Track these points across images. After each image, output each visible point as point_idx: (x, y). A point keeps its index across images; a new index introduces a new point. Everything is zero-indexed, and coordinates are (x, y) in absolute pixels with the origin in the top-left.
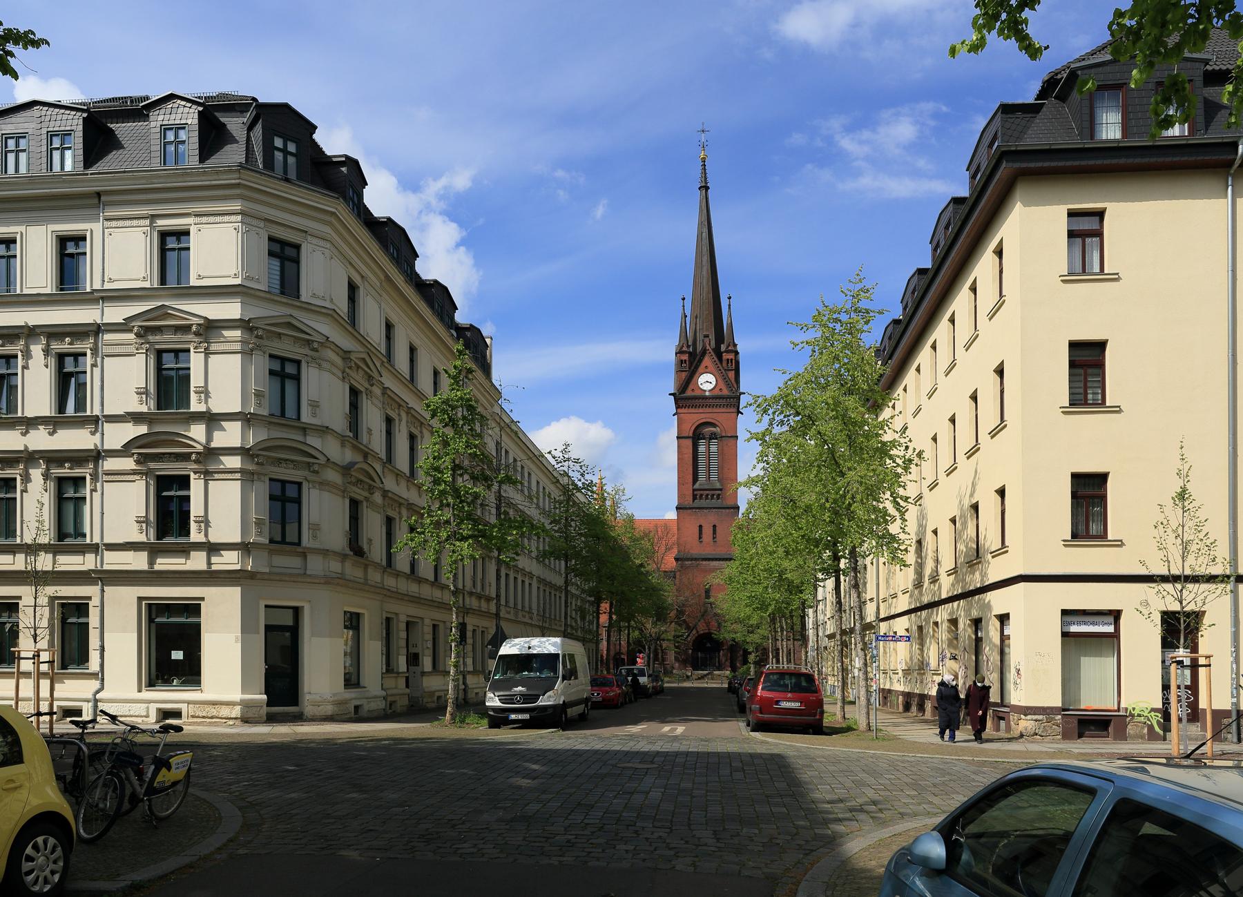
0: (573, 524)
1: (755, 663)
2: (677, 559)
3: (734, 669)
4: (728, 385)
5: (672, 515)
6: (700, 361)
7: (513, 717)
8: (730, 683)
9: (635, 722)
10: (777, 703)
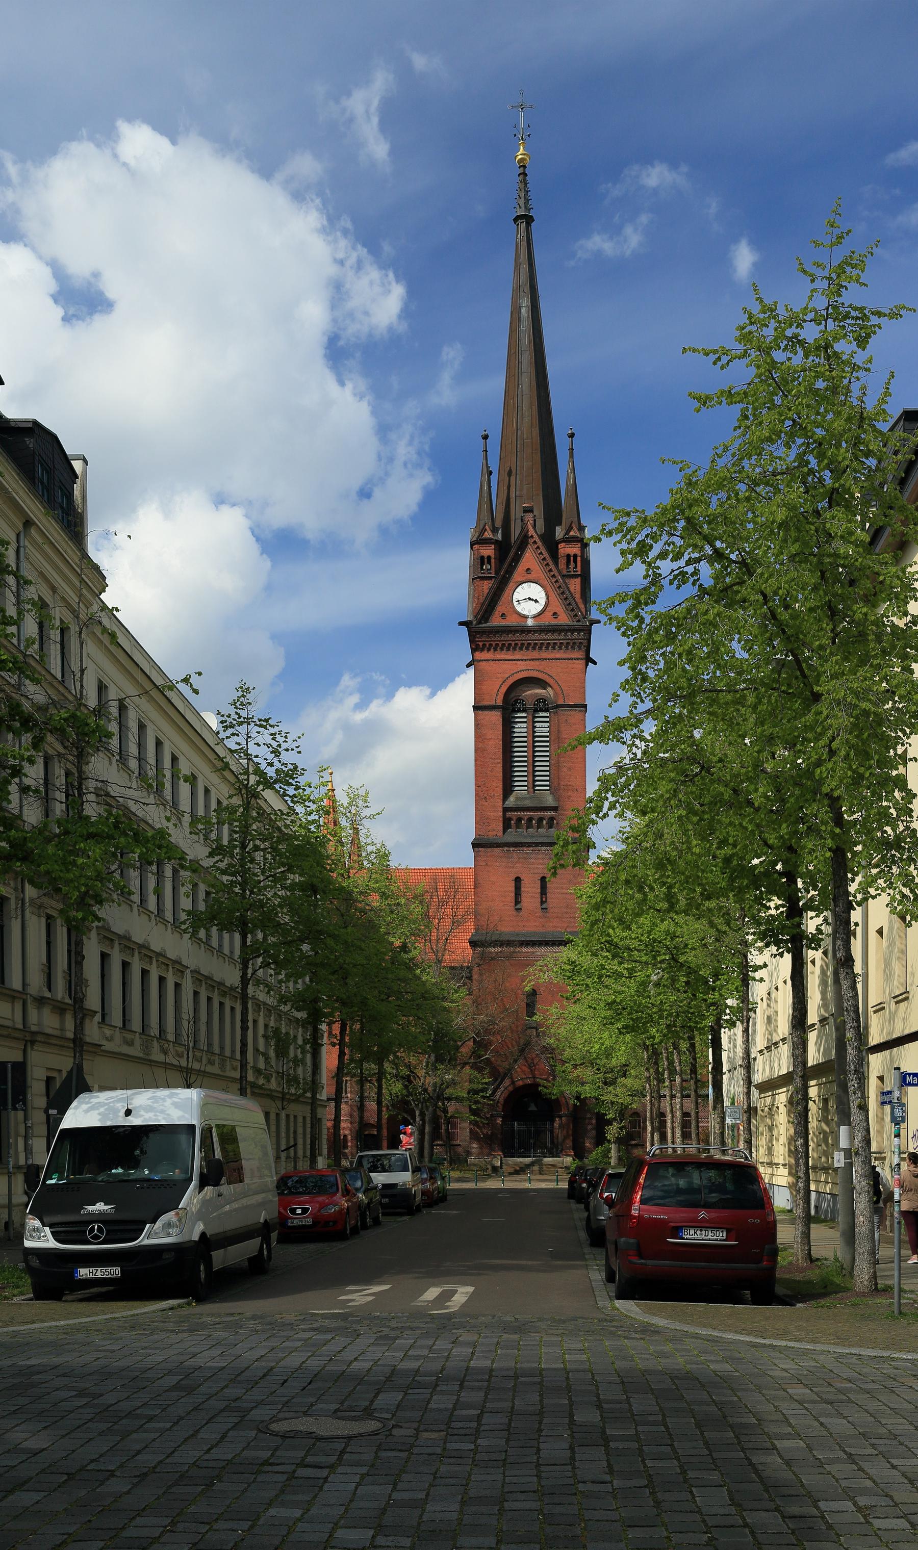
0: (258, 856)
1: (619, 1141)
2: (473, 944)
3: (580, 1153)
4: (569, 605)
5: (465, 859)
6: (517, 559)
7: (84, 1273)
8: (571, 1182)
9: (368, 1279)
10: (676, 1232)
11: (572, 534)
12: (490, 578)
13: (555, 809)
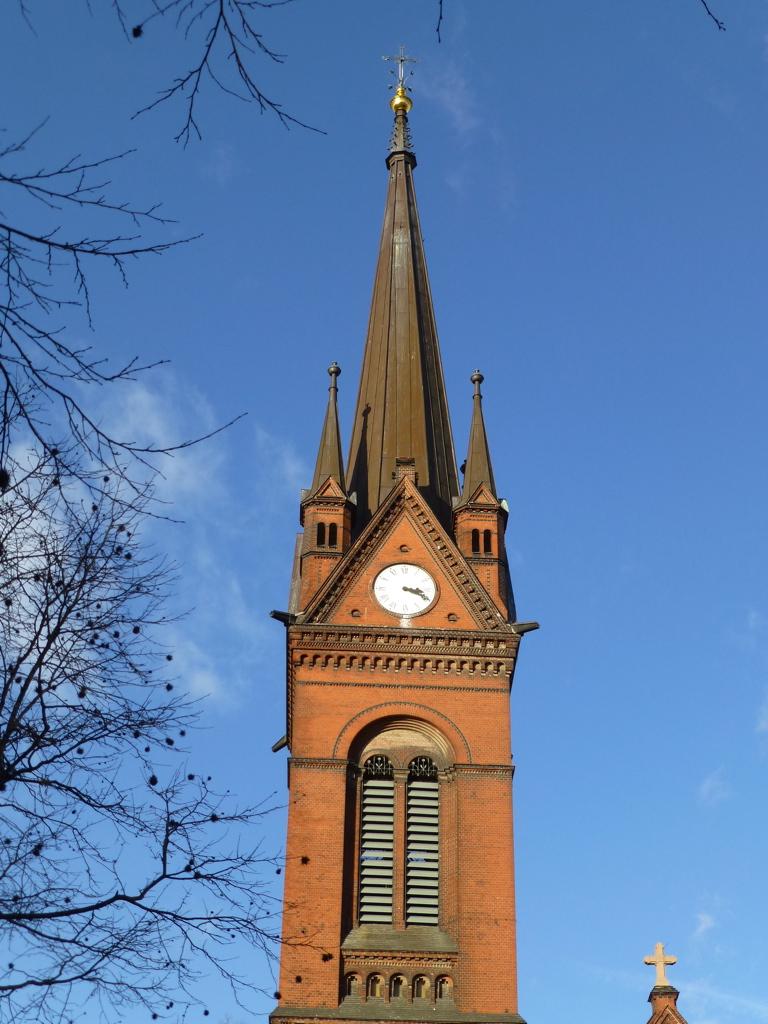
11: (481, 500)
12: (333, 556)
13: (451, 956)
